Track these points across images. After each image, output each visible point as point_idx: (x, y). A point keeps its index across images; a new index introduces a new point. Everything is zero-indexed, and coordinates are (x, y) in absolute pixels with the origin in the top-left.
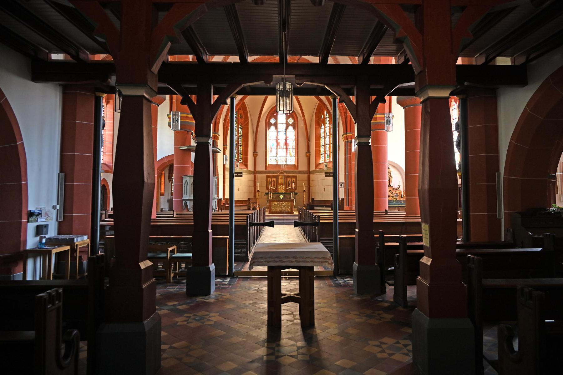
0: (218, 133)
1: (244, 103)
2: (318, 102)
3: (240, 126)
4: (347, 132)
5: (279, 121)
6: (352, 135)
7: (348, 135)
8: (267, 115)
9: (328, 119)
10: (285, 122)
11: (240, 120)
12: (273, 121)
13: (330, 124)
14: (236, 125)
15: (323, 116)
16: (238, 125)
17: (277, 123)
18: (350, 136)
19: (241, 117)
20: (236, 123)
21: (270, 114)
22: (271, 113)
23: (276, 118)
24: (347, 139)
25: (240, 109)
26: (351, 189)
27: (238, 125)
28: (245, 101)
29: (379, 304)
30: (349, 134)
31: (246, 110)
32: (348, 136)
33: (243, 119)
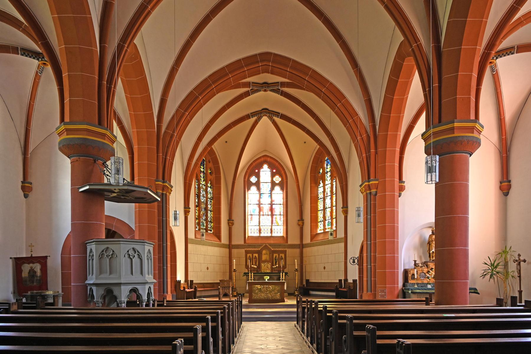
3: (209, 185)
4: (369, 178)
5: (262, 180)
6: (377, 182)
7: (371, 183)
9: (329, 174)
13: (332, 179)
15: (321, 171)
16: (207, 183)
20: (204, 181)
23: (258, 176)
24: (370, 189)
25: (209, 162)
26: (375, 266)
27: (207, 183)
28: (213, 147)
30: (373, 180)
31: (218, 163)
32: (371, 184)
33: (214, 175)
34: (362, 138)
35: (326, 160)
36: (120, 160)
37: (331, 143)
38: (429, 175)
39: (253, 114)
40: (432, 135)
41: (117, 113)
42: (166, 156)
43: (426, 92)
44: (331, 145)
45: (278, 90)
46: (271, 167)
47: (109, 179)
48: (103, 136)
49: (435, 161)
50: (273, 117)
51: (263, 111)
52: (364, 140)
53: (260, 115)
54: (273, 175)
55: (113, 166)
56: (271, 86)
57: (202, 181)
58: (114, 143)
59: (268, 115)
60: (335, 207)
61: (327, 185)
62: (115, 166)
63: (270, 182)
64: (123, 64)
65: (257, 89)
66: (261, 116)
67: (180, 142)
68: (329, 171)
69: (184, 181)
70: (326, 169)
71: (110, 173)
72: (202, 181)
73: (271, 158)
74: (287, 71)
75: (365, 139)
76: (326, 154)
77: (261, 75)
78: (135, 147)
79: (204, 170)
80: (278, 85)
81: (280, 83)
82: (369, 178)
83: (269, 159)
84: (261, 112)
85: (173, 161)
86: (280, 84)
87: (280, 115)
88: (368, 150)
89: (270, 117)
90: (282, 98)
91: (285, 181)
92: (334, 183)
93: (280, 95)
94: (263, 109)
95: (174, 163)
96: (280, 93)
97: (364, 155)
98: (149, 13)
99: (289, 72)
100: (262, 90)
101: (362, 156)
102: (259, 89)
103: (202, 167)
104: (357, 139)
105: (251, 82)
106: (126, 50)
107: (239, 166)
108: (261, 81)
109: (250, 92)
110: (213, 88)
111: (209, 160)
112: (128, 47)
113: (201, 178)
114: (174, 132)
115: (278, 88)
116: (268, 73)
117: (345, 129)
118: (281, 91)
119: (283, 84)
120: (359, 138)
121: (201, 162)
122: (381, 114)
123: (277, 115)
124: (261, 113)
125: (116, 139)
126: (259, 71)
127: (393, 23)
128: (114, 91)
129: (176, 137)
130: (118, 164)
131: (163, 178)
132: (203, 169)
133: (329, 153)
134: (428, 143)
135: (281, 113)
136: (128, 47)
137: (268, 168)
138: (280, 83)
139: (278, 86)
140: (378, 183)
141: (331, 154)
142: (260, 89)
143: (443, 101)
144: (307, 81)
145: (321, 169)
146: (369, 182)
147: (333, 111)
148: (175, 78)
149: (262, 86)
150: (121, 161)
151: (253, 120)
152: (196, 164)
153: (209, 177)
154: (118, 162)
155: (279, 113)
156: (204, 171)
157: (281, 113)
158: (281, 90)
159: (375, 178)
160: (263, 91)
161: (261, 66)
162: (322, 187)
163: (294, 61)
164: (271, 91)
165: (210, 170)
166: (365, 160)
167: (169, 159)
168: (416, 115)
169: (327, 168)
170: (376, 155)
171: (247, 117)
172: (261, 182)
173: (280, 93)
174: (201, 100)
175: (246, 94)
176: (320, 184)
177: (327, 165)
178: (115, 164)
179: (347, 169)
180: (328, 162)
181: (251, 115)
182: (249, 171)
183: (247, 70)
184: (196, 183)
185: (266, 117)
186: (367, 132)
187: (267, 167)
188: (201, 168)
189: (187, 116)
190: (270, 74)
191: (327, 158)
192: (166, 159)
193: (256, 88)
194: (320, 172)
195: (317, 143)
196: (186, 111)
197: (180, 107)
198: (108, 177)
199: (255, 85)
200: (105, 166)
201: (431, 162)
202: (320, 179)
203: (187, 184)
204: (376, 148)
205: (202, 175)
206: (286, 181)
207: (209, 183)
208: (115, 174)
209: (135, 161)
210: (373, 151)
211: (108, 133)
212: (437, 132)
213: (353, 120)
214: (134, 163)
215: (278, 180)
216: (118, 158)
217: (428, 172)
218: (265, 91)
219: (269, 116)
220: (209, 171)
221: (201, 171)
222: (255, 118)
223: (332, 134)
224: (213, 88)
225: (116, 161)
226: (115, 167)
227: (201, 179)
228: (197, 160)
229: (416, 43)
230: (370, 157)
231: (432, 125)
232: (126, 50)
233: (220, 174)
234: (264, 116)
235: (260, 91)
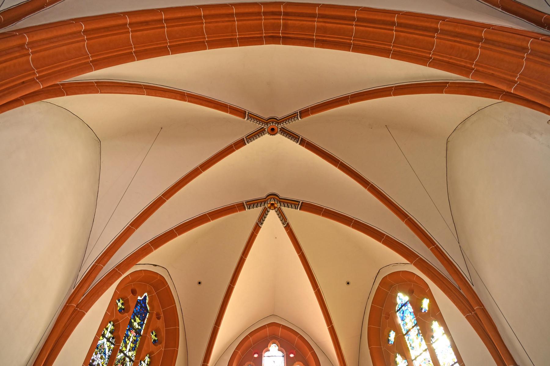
20: (133, 349)
25: (159, 318)
33: (162, 347)
51: (269, 197)
57: (128, 347)
61: (415, 359)
72: (128, 347)
73: (284, 327)
79: (140, 327)
80: (297, 204)
87: (300, 204)
93: (300, 144)
132: (141, 325)
137: (279, 350)
157: (301, 202)
165: (155, 336)
187: (277, 348)
220: (153, 337)
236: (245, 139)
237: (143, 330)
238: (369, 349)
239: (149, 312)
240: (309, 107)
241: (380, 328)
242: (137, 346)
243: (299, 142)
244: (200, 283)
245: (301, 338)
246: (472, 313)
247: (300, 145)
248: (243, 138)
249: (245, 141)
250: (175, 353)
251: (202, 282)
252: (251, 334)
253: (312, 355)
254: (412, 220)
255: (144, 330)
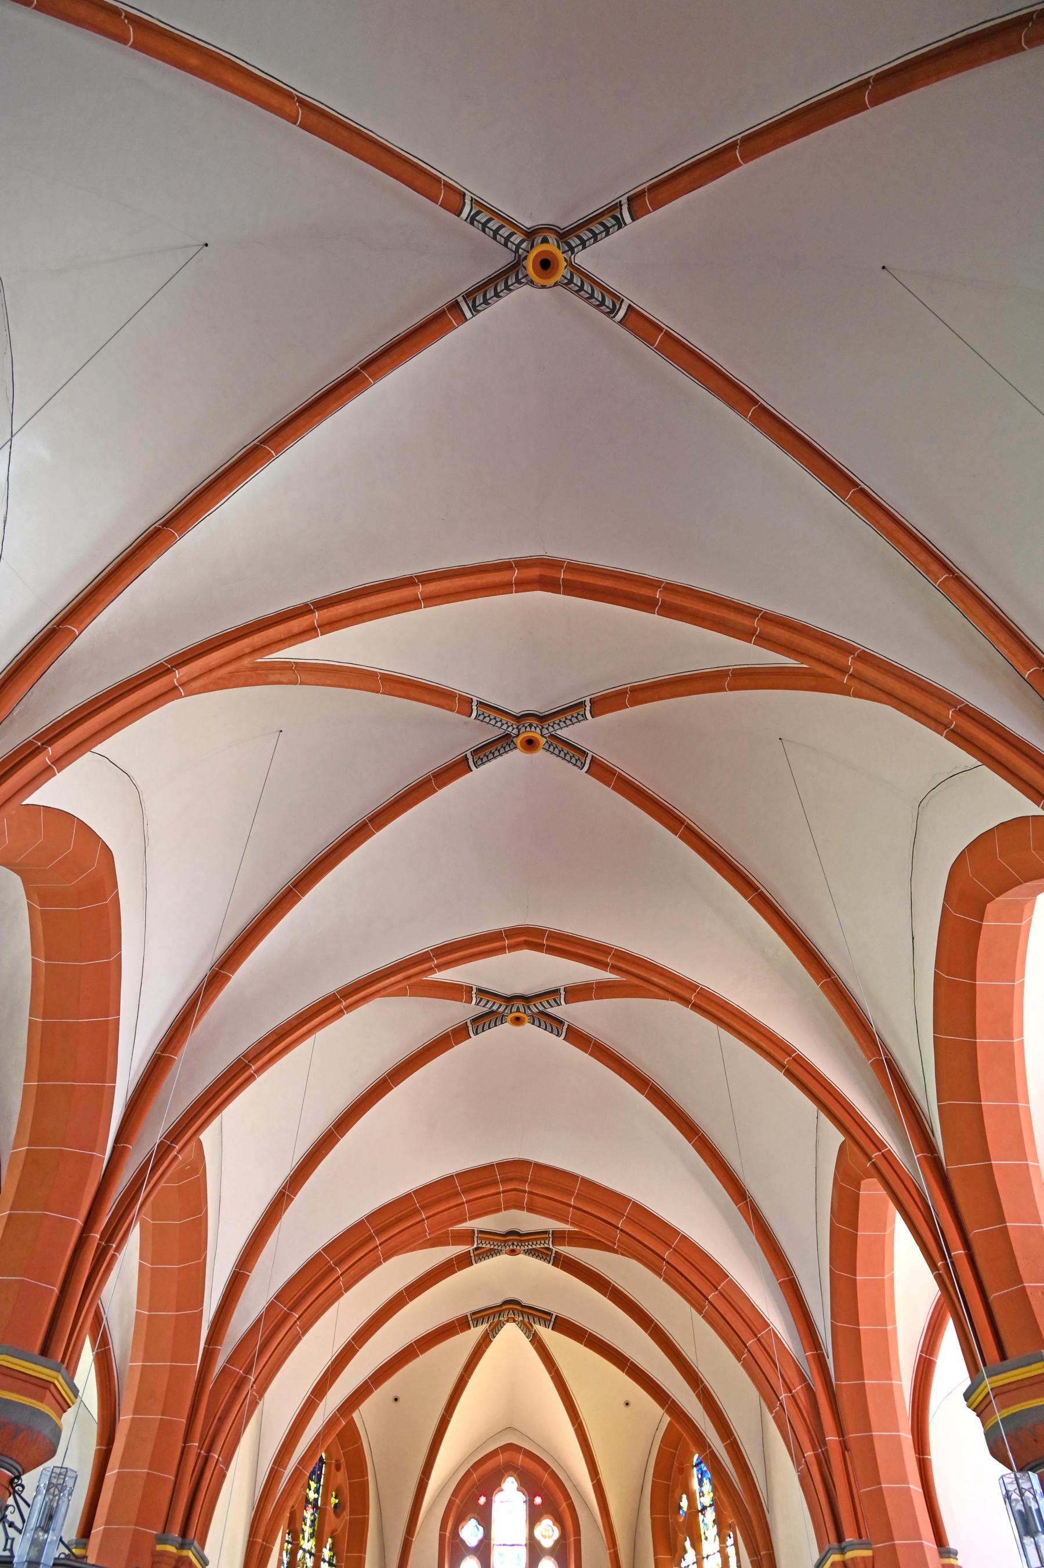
0: (203, 1543)
1: (352, 1425)
2: (667, 1419)
3: (326, 1553)
4: (840, 1538)
5: (497, 1535)
6: (868, 1553)
7: (850, 1555)
8: (450, 1503)
9: (710, 1515)
10: (522, 1537)
11: (332, 1521)
12: (471, 1533)
13: (722, 1536)
14: (313, 1542)
15: (684, 1504)
16: (319, 1546)
17: (490, 1543)
18: (863, 1558)
19: (336, 1505)
20: (312, 1535)
21: (460, 1496)
22: (463, 1491)
23: (485, 1519)
25: (338, 1468)
27: (319, 1546)
28: (355, 1415)
29: (281, 1536)
30: (853, 1546)
31: (364, 1472)
32: (853, 1559)
33: (346, 1516)
34: (793, 1396)
35: (697, 1465)
36: (70, 1477)
37: (704, 1408)
38: (1028, 1541)
39: (479, 1316)
40: (994, 1398)
41: (105, 1321)
42: (209, 1450)
43: (939, 1271)
44: (705, 1413)
45: (545, 1251)
46: (530, 1485)
47: (13, 1539)
48: (41, 1387)
49: (1032, 1491)
50: (532, 1326)
52: (801, 1406)
53: (496, 1320)
54: (534, 1517)
55: (40, 1498)
56: (528, 1241)
58: (65, 1411)
59: (521, 1318)
60: (733, 1547)
62: (47, 1499)
63: (524, 1543)
64: (162, 1184)
65: (492, 1247)
66: (499, 1321)
67: (261, 1403)
68: (708, 1505)
69: (250, 1536)
70: (700, 1497)
71: (24, 1521)
73: (528, 1454)
74: (569, 1205)
75: (803, 1400)
76: (691, 1444)
77: (503, 1213)
78: (125, 1418)
79: (316, 1496)
80: (546, 1238)
81: (551, 1233)
82: (840, 1538)
83: (521, 1459)
84: (499, 1309)
85: (227, 1469)
86: (550, 1236)
88: (819, 1439)
89: (525, 1324)
90: (558, 1271)
91: (572, 1539)
92: (731, 1551)
94: (507, 1302)
95: (230, 1473)
96: (552, 1258)
97: (809, 1453)
98: (250, 1079)
99: (574, 1207)
100: (504, 1252)
101: (804, 1457)
102: (496, 1247)
103: (313, 1485)
104: (779, 1400)
105: (476, 1230)
106: (176, 1157)
107: (427, 1483)
108: (503, 1229)
109: (472, 1255)
110: (377, 1247)
111: (337, 1461)
112: (179, 1151)
113: (306, 1525)
114: (248, 1371)
115: (546, 1246)
116: (522, 1208)
117: (738, 1365)
118: (553, 1255)
119: (559, 1237)
120: (783, 1396)
121: (311, 1469)
122: (832, 1324)
123: (545, 1320)
124: (500, 1313)
125: (76, 1396)
126: (499, 1204)
127: (811, 1106)
128: (114, 1258)
129: (252, 1386)
130: (57, 1492)
131: (184, 1534)
132: (317, 1491)
133: (701, 1443)
134: (991, 1423)
135: (555, 1314)
136: (179, 1151)
137: (518, 1490)
138: (551, 1233)
139: (547, 1242)
140: (873, 1557)
141: (710, 1447)
142: (500, 1248)
143: (992, 1296)
144: (621, 1230)
145: (684, 1496)
146: (842, 1551)
147: (700, 1313)
148: (281, 1218)
149: (505, 1242)
150: (69, 1483)
151: (475, 1333)
152: (297, 1473)
153: (332, 1521)
154: (57, 1486)
155: (549, 1314)
156: (316, 1500)
157: (555, 1314)
158: (554, 1252)
159: (860, 1537)
160: (506, 1253)
161: (503, 1192)
162: (694, 1563)
163: (586, 1182)
164: (528, 1252)
165: (336, 1498)
166: (814, 1469)
167: (216, 1460)
168: (932, 1327)
169: (702, 1494)
170: (846, 1453)
171: (461, 1324)
172: (495, 1543)
173: (552, 1258)
174: (339, 1277)
175: (463, 1261)
176: (685, 1552)
177: (701, 1483)
178: (48, 1490)
179: (766, 1501)
180: (703, 1473)
181: (474, 1317)
182: (457, 1501)
183: (467, 1202)
184: (286, 1544)
185: (514, 1324)
186: (803, 1378)
187: (516, 1485)
188: (310, 1489)
189: (296, 1322)
190: (525, 1213)
191: (696, 1456)
192: (206, 1459)
193: (488, 1246)
194: (680, 1508)
195: (662, 1406)
196: (293, 1308)
197: (279, 1297)
198: (11, 1532)
199: (486, 1239)
200: (13, 1488)
201: (1022, 1495)
202: (682, 1533)
203: (257, 1548)
204: (841, 1431)
205: (308, 1514)
206: (567, 1505)
207: (328, 1546)
208: (36, 1529)
209: (109, 1466)
210: (832, 1438)
211: (58, 1381)
212: (1007, 1388)
213: (759, 1340)
214: (106, 1475)
215: (551, 1533)
216: (63, 1470)
217: (1022, 1534)
218: (513, 1252)
219: (523, 1322)
221: (307, 1501)
222: (482, 1328)
223: (702, 1377)
224: (377, 1247)
225: (54, 1481)
226: (46, 1503)
227: (303, 1531)
228: (302, 1461)
229: (880, 1150)
230: (828, 1461)
231: (985, 1364)
232: (176, 1157)
233: (365, 1510)
234: (507, 1321)
235: (498, 1252)
236: (469, 756)
237: (320, 1498)
238: (651, 1518)
239: (325, 1463)
240: (626, 686)
241: (670, 1484)
242: (316, 1528)
243: (552, 1261)
244: (396, 1399)
245: (553, 1475)
246: (758, 1557)
247: (553, 1267)
248: (466, 755)
249: (468, 762)
250: (364, 1523)
251: (400, 1399)
252: (476, 1466)
253: (568, 1508)
254: (707, 1392)
255: (321, 1497)
